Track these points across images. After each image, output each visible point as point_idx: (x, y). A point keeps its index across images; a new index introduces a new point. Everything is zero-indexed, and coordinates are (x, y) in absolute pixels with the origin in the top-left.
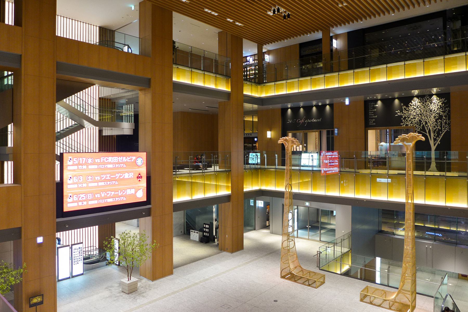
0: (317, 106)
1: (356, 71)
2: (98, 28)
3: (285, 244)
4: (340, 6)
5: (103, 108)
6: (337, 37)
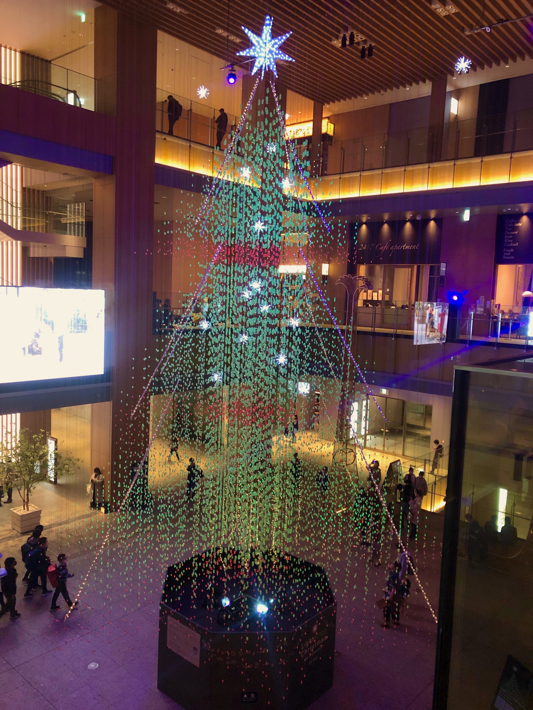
0: (413, 221)
1: (486, 159)
2: (18, 54)
3: (339, 456)
4: (468, 33)
5: (29, 207)
6: (458, 93)
